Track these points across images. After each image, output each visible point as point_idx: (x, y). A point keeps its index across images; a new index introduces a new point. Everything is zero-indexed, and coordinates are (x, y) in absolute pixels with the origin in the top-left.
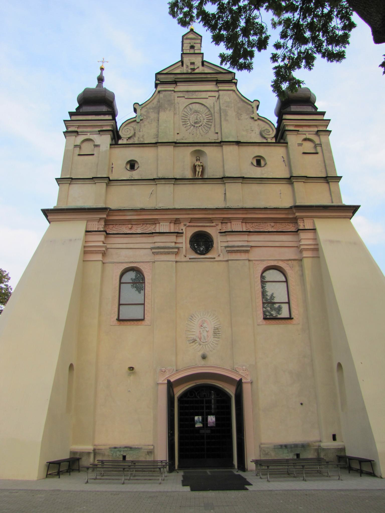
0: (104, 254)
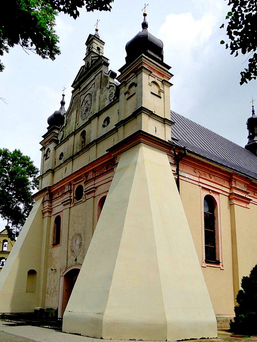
0: (50, 212)
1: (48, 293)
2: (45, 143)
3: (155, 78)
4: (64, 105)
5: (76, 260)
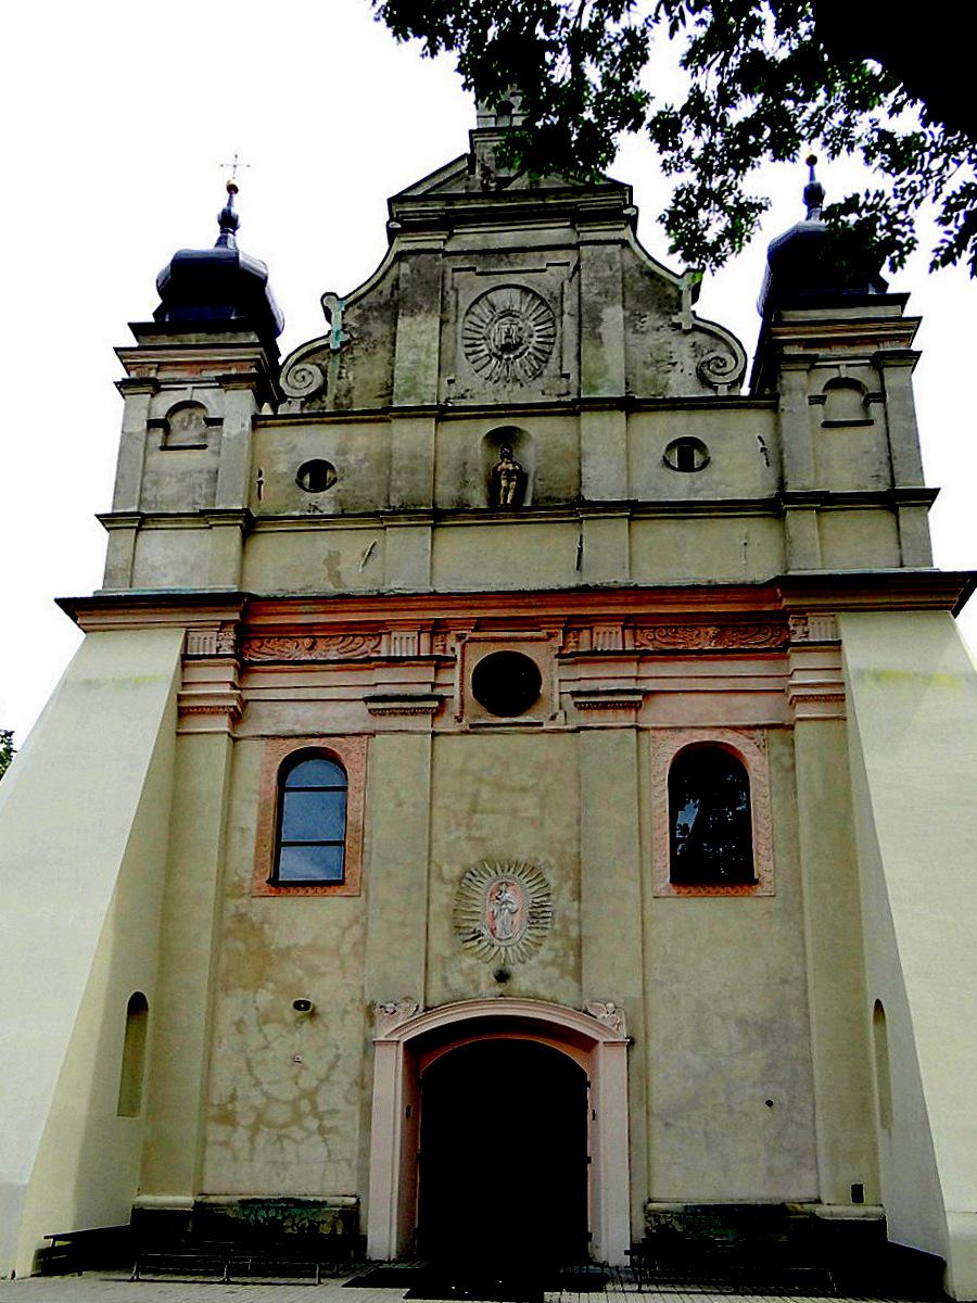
0: (236, 718)
1: (227, 1118)
2: (160, 364)
4: (237, 232)
5: (502, 977)
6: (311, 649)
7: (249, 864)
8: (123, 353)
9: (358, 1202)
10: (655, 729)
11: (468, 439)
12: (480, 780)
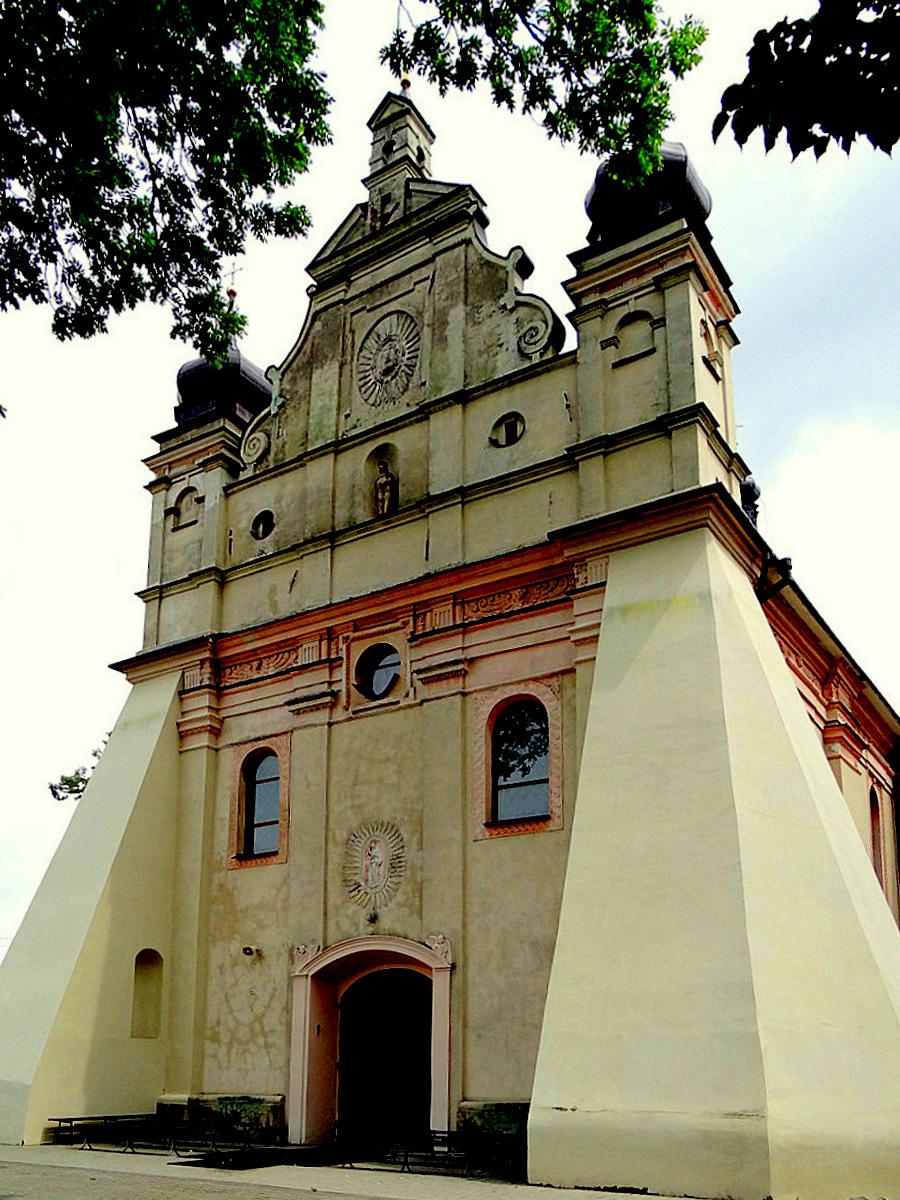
0: (216, 732)
1: (215, 1039)
2: (169, 463)
3: (704, 309)
5: (373, 919)
6: (259, 668)
7: (225, 846)
8: (149, 462)
9: (283, 1099)
10: (475, 691)
11: (356, 464)
12: (360, 757)
